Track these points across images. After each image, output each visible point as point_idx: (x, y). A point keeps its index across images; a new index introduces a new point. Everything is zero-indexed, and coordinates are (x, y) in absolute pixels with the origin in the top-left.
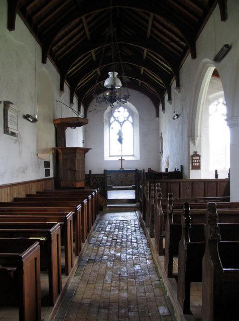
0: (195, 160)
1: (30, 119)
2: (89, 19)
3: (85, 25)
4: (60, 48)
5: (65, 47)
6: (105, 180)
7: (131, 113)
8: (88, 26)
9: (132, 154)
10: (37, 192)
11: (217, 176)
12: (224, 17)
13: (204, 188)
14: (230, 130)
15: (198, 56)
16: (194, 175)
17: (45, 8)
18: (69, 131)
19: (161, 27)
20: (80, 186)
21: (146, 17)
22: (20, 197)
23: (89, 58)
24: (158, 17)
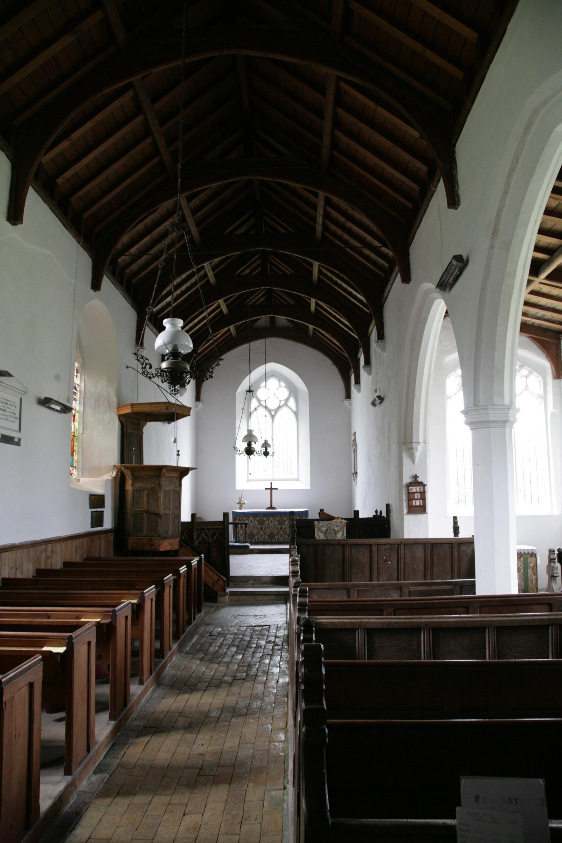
0: (416, 498)
1: (53, 406)
2: (195, 202)
3: (187, 213)
4: (135, 258)
5: (145, 257)
6: (214, 540)
7: (293, 391)
8: (193, 215)
9: (296, 477)
10: (66, 564)
11: (456, 530)
12: (453, 201)
13: (425, 555)
14: (473, 433)
15: (413, 276)
16: (413, 528)
17: (100, 179)
18: (152, 431)
19: (342, 219)
20: (168, 548)
21: (312, 198)
22: (19, 576)
23: (201, 279)
24: (335, 199)
